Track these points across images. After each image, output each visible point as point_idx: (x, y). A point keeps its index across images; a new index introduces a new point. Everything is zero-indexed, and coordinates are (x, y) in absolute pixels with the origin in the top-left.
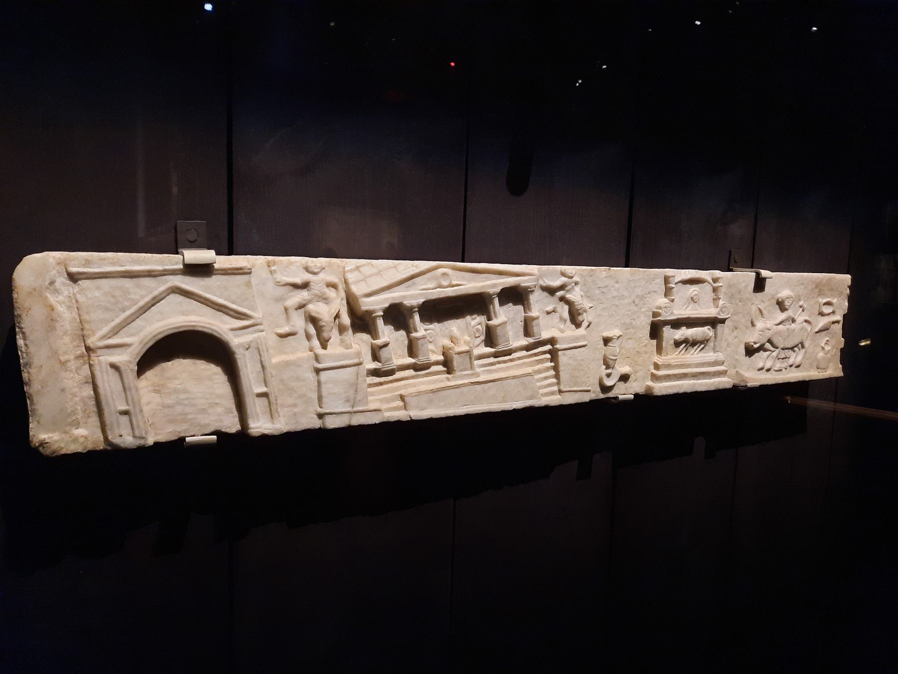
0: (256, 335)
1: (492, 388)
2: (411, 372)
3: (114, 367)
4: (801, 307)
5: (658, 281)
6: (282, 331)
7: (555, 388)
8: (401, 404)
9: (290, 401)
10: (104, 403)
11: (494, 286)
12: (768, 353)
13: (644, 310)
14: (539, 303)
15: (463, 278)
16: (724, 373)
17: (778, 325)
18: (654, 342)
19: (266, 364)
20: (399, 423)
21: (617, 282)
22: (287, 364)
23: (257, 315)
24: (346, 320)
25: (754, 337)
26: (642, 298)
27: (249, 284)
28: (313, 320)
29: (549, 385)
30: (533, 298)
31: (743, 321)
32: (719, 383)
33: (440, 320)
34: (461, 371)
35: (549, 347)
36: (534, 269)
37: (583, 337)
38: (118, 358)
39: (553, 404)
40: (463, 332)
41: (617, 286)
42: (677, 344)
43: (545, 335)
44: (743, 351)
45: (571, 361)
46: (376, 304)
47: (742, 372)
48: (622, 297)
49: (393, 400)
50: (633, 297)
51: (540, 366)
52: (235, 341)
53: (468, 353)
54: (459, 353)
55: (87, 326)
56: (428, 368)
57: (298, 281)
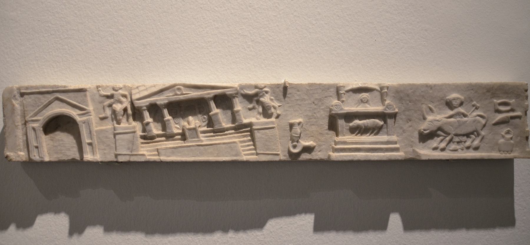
0: (88, 117)
1: (211, 149)
3: (34, 129)
5: (332, 90)
7: (254, 152)
8: (156, 153)
10: (29, 143)
11: (209, 94)
12: (441, 138)
19: (92, 130)
21: (298, 91)
22: (102, 131)
24: (130, 112)
25: (424, 127)
26: (320, 100)
27: (85, 96)
28: (114, 112)
29: (250, 150)
31: (415, 115)
32: (390, 155)
34: (192, 138)
35: (249, 129)
37: (272, 123)
38: (35, 125)
39: (251, 160)
41: (298, 93)
43: (245, 121)
45: (263, 136)
47: (418, 150)
48: (304, 100)
49: (154, 151)
50: (312, 100)
51: (245, 139)
53: (195, 129)
55: (26, 112)
56: (224, 132)
57: (109, 94)
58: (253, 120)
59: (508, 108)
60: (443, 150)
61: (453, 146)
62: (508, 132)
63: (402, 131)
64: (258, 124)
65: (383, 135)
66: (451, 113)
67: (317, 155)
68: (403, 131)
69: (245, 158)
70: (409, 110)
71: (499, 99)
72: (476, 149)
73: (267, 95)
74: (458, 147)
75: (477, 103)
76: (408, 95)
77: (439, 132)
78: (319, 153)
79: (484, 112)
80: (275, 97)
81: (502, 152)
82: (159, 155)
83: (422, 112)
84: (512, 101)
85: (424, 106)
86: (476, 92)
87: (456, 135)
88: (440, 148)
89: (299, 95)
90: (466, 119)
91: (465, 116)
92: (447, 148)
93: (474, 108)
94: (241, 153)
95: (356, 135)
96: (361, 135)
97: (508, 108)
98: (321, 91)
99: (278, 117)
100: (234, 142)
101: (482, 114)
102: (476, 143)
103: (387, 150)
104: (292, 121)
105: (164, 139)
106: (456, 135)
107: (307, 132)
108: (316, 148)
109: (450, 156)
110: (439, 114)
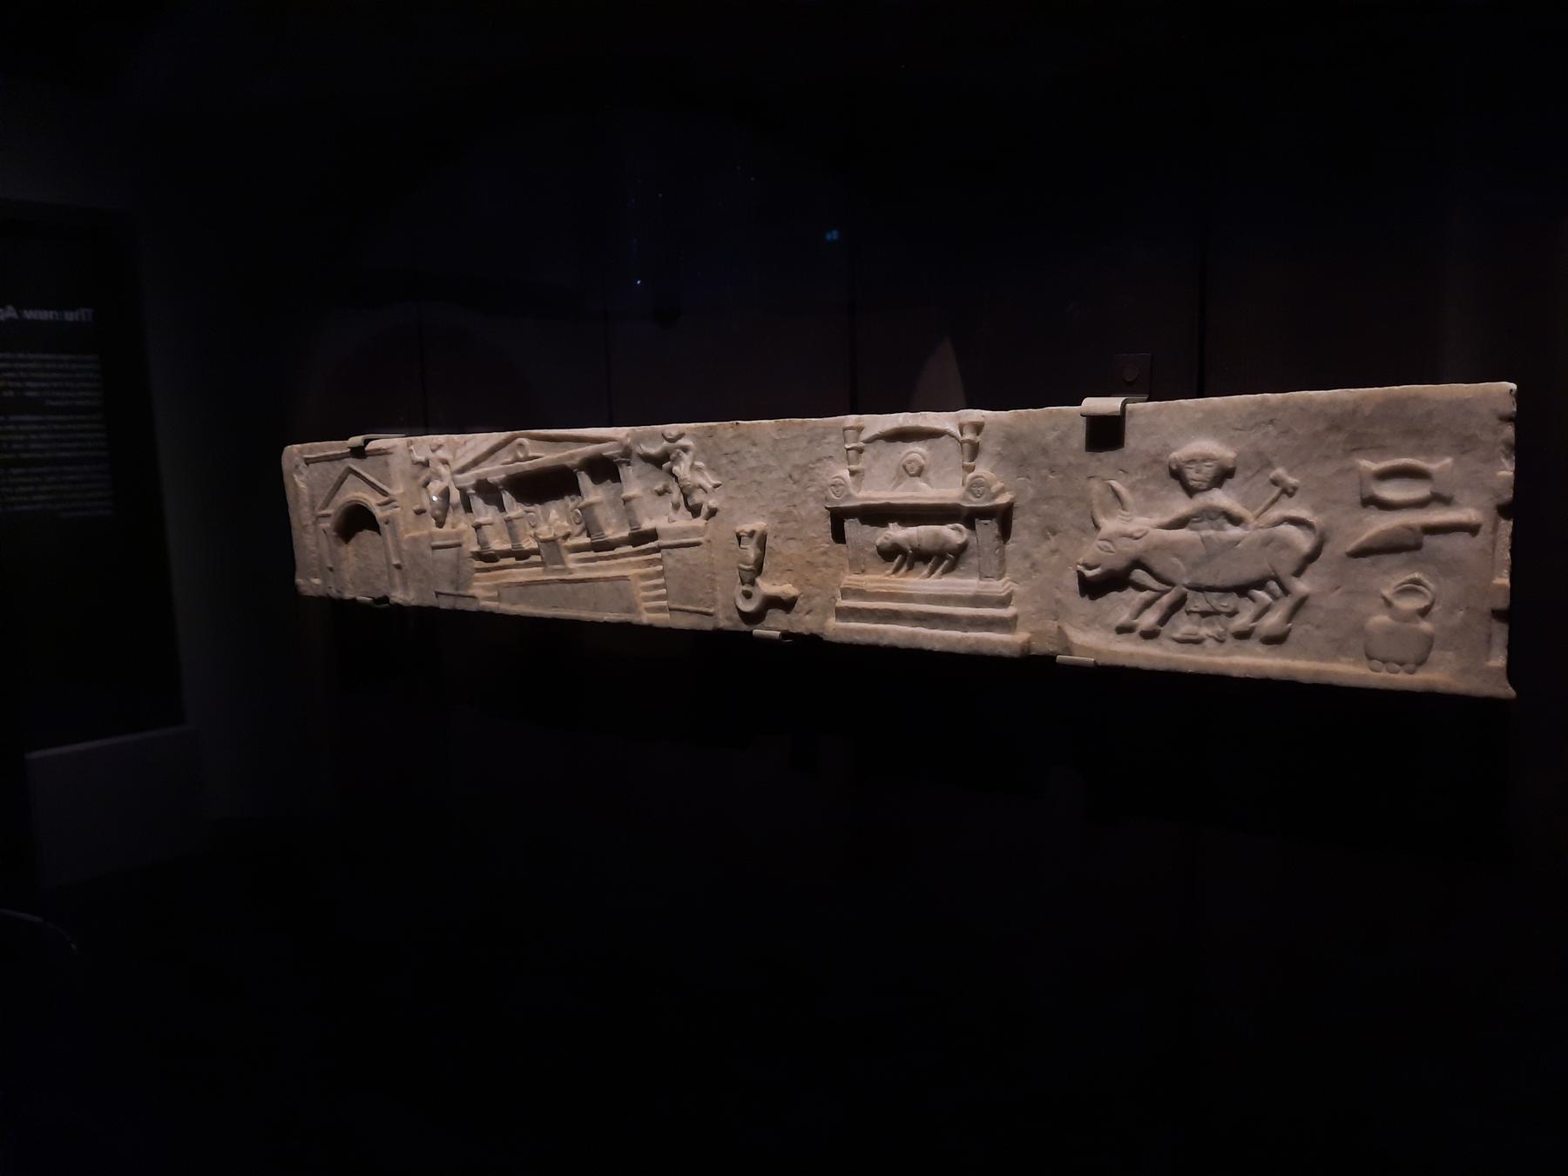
5: (833, 438)
11: (572, 457)
12: (1146, 595)
13: (812, 490)
14: (635, 483)
16: (1007, 624)
21: (754, 445)
25: (1094, 554)
26: (805, 469)
27: (386, 464)
30: (625, 472)
31: (1069, 515)
32: (978, 641)
36: (621, 433)
37: (696, 531)
39: (658, 624)
41: (754, 450)
44: (1074, 584)
45: (679, 566)
48: (766, 469)
50: (788, 468)
51: (651, 569)
59: (1419, 491)
60: (1150, 635)
61: (1184, 625)
63: (1027, 565)
65: (967, 574)
66: (1182, 506)
67: (802, 622)
68: (1033, 565)
69: (646, 618)
70: (1049, 499)
71: (1382, 458)
72: (1275, 640)
73: (685, 456)
74: (1204, 631)
75: (1290, 471)
76: (1045, 451)
77: (1139, 575)
78: (808, 617)
79: (1316, 509)
80: (708, 462)
81: (1376, 663)
83: (1090, 505)
84: (1438, 465)
85: (1096, 486)
86: (1285, 432)
87: (1199, 589)
89: (756, 456)
90: (1234, 532)
91: (1236, 521)
92: (1165, 630)
93: (1277, 490)
94: (637, 606)
95: (896, 571)
96: (945, 572)
97: (1419, 491)
98: (804, 443)
100: (624, 578)
101: (1303, 513)
105: (512, 560)
106: (1199, 589)
108: (800, 602)
109: (1168, 659)
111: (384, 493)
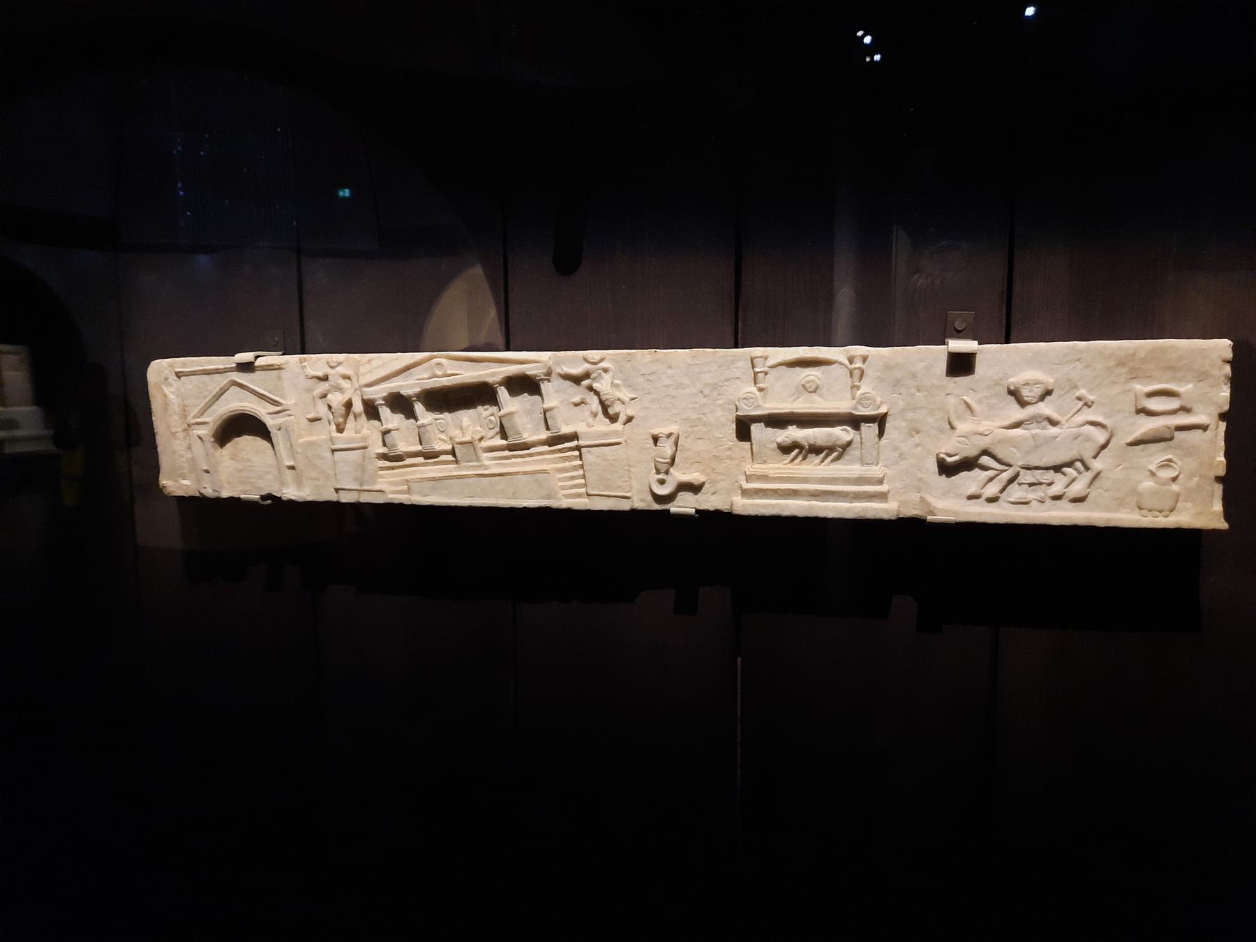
1: (500, 483)
2: (421, 460)
4: (1079, 399)
5: (740, 364)
6: (310, 416)
9: (314, 475)
11: (493, 375)
12: (990, 473)
15: (461, 367)
16: (883, 496)
17: (284, 421)
18: (746, 445)
20: (401, 506)
21: (670, 368)
22: (311, 444)
23: (288, 402)
25: (954, 447)
26: (715, 387)
27: (279, 378)
31: (931, 420)
32: (864, 509)
33: (451, 410)
36: (545, 356)
37: (616, 433)
40: (469, 423)
41: (670, 372)
42: (785, 449)
45: (599, 461)
46: (378, 393)
47: (931, 499)
48: (680, 386)
51: (567, 464)
52: (270, 422)
54: (461, 443)
57: (320, 374)
58: (580, 428)
59: (1173, 404)
60: (992, 500)
61: (1016, 492)
62: (1167, 464)
64: (588, 435)
65: (851, 462)
66: (1018, 414)
68: (901, 454)
70: (915, 409)
75: (1090, 391)
76: (914, 376)
77: (985, 460)
79: (1106, 416)
80: (625, 380)
82: (409, 491)
83: (947, 412)
85: (952, 400)
88: (984, 497)
90: (1053, 430)
91: (1053, 423)
92: (1003, 496)
93: (1081, 403)
97: (1173, 404)
99: (630, 419)
100: (544, 472)
102: (1077, 488)
103: (858, 496)
104: (655, 431)
107: (688, 453)
110: (987, 418)
111: (275, 403)
